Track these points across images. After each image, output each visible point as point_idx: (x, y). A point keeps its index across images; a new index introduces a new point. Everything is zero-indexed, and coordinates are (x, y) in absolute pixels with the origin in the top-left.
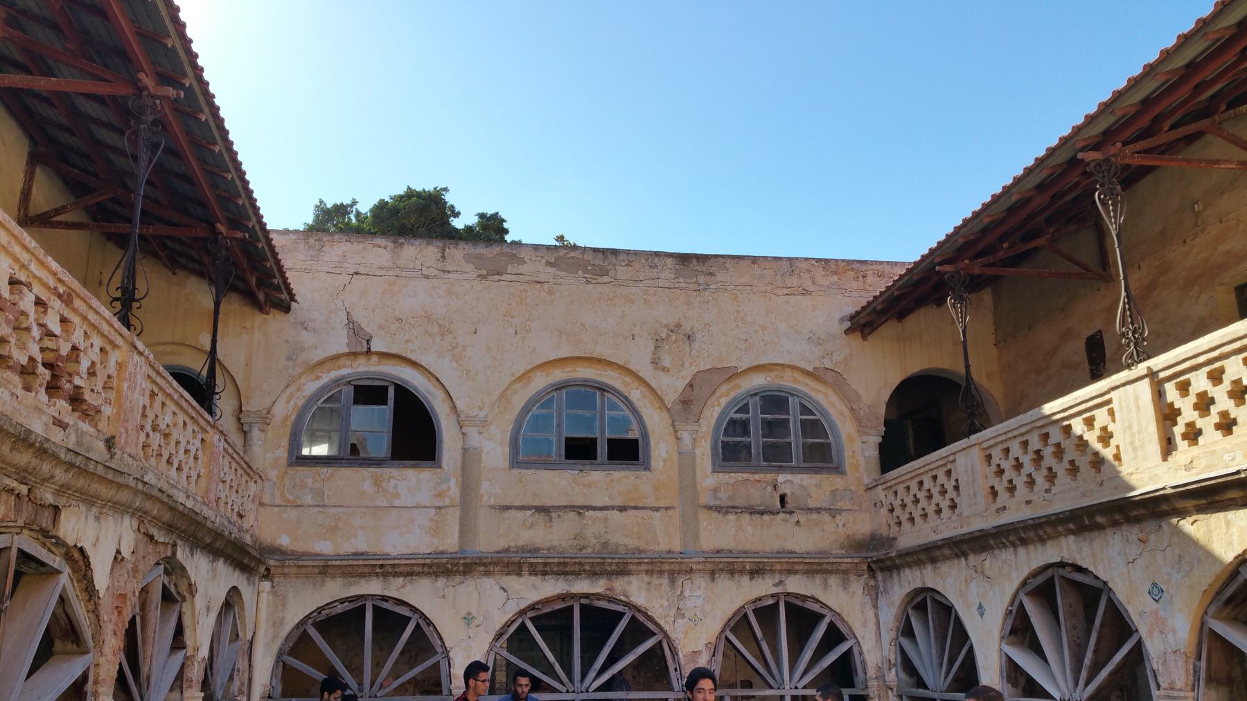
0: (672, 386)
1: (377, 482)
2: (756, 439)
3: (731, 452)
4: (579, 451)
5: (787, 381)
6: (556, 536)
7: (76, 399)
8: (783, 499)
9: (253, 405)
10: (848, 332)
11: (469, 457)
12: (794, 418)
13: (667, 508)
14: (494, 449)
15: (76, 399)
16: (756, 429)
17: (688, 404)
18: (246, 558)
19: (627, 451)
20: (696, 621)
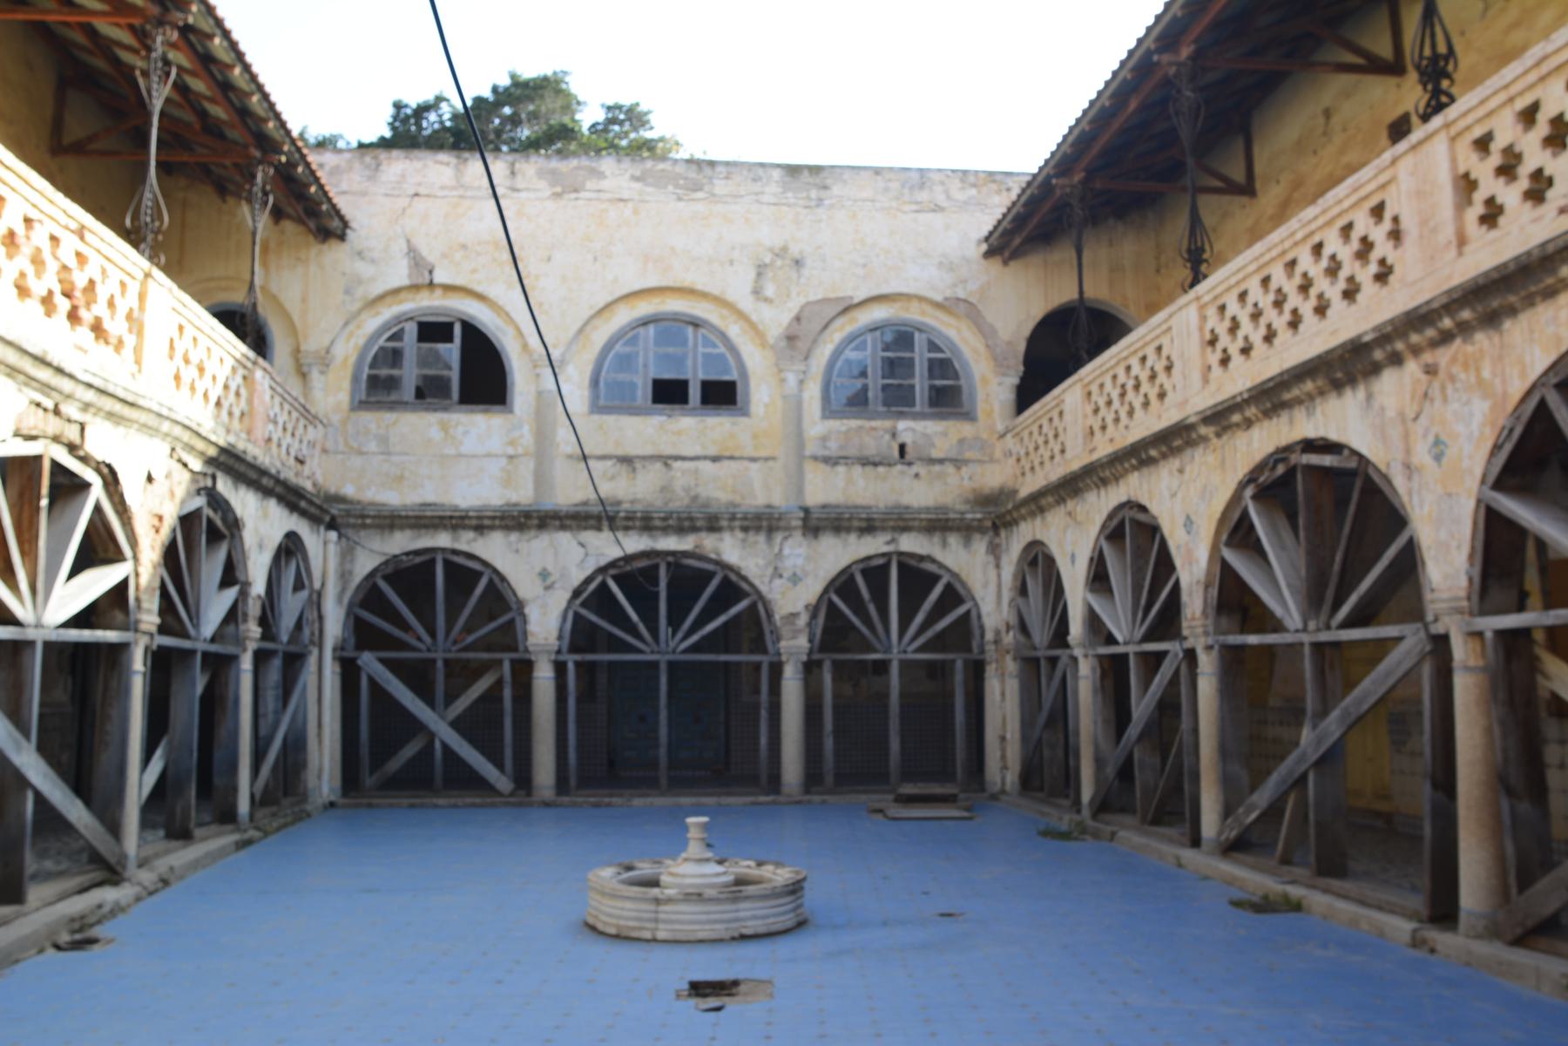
0: (776, 319)
1: (444, 428)
4: (669, 393)
5: (914, 314)
7: (97, 328)
8: (902, 448)
10: (989, 254)
12: (920, 356)
13: (767, 459)
15: (97, 328)
17: (794, 341)
19: (722, 394)
20: (795, 579)
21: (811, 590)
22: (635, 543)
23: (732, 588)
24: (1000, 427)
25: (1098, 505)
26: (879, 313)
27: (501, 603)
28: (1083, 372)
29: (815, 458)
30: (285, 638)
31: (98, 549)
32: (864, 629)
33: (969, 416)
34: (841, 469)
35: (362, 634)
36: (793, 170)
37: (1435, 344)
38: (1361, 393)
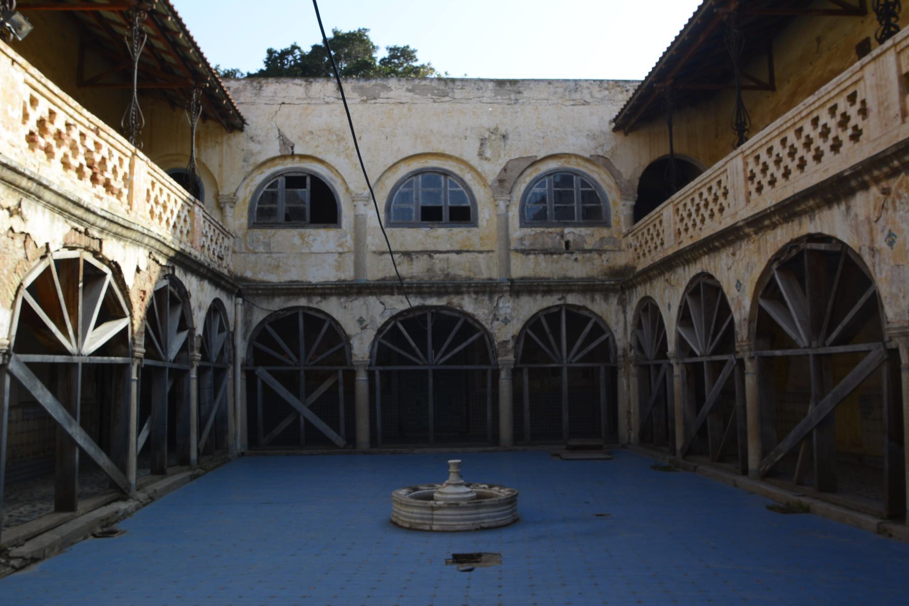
0: (491, 170)
1: (302, 237)
4: (430, 215)
5: (573, 165)
7: (107, 185)
8: (567, 243)
10: (615, 130)
11: (359, 222)
13: (488, 252)
15: (107, 185)
17: (503, 183)
19: (463, 215)
20: (506, 321)
21: (515, 327)
22: (415, 302)
23: (470, 325)
24: (624, 230)
26: (552, 165)
27: (336, 336)
29: (516, 251)
31: (111, 311)
32: (546, 350)
34: (532, 257)
35: (257, 356)
36: (500, 83)
37: (888, 176)
38: (843, 207)
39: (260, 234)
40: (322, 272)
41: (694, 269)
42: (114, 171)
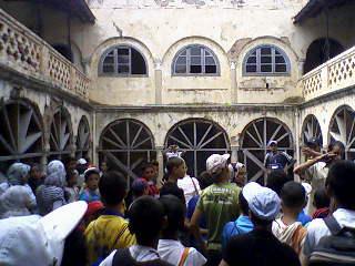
0: (227, 46)
1: (127, 82)
2: (258, 64)
3: (250, 68)
4: (196, 70)
6: (187, 99)
7: (29, 62)
9: (85, 56)
10: (295, 23)
11: (158, 74)
12: (273, 55)
14: (166, 70)
15: (29, 62)
16: (116, 59)
18: (88, 107)
19: (212, 69)
20: (235, 126)
21: (240, 129)
22: (186, 116)
23: (216, 128)
25: (332, 106)
26: (261, 42)
27: (146, 133)
28: (328, 62)
30: (62, 147)
31: (33, 128)
33: (289, 75)
35: (104, 144)
39: (106, 80)
40: (140, 102)
41: (341, 102)
42: (33, 54)
